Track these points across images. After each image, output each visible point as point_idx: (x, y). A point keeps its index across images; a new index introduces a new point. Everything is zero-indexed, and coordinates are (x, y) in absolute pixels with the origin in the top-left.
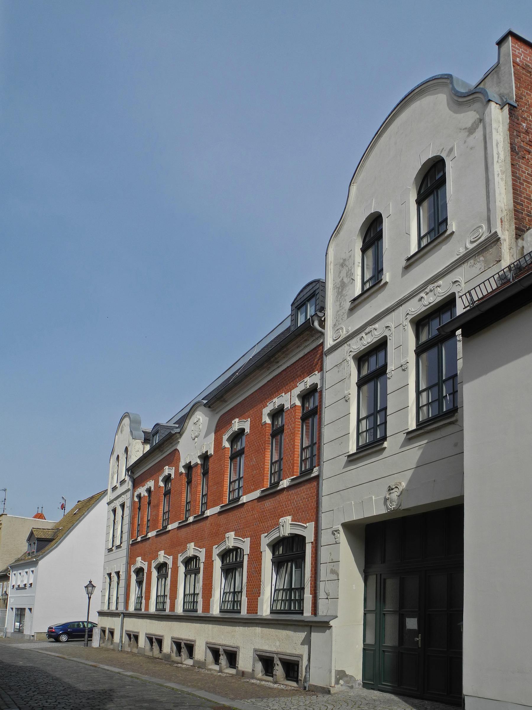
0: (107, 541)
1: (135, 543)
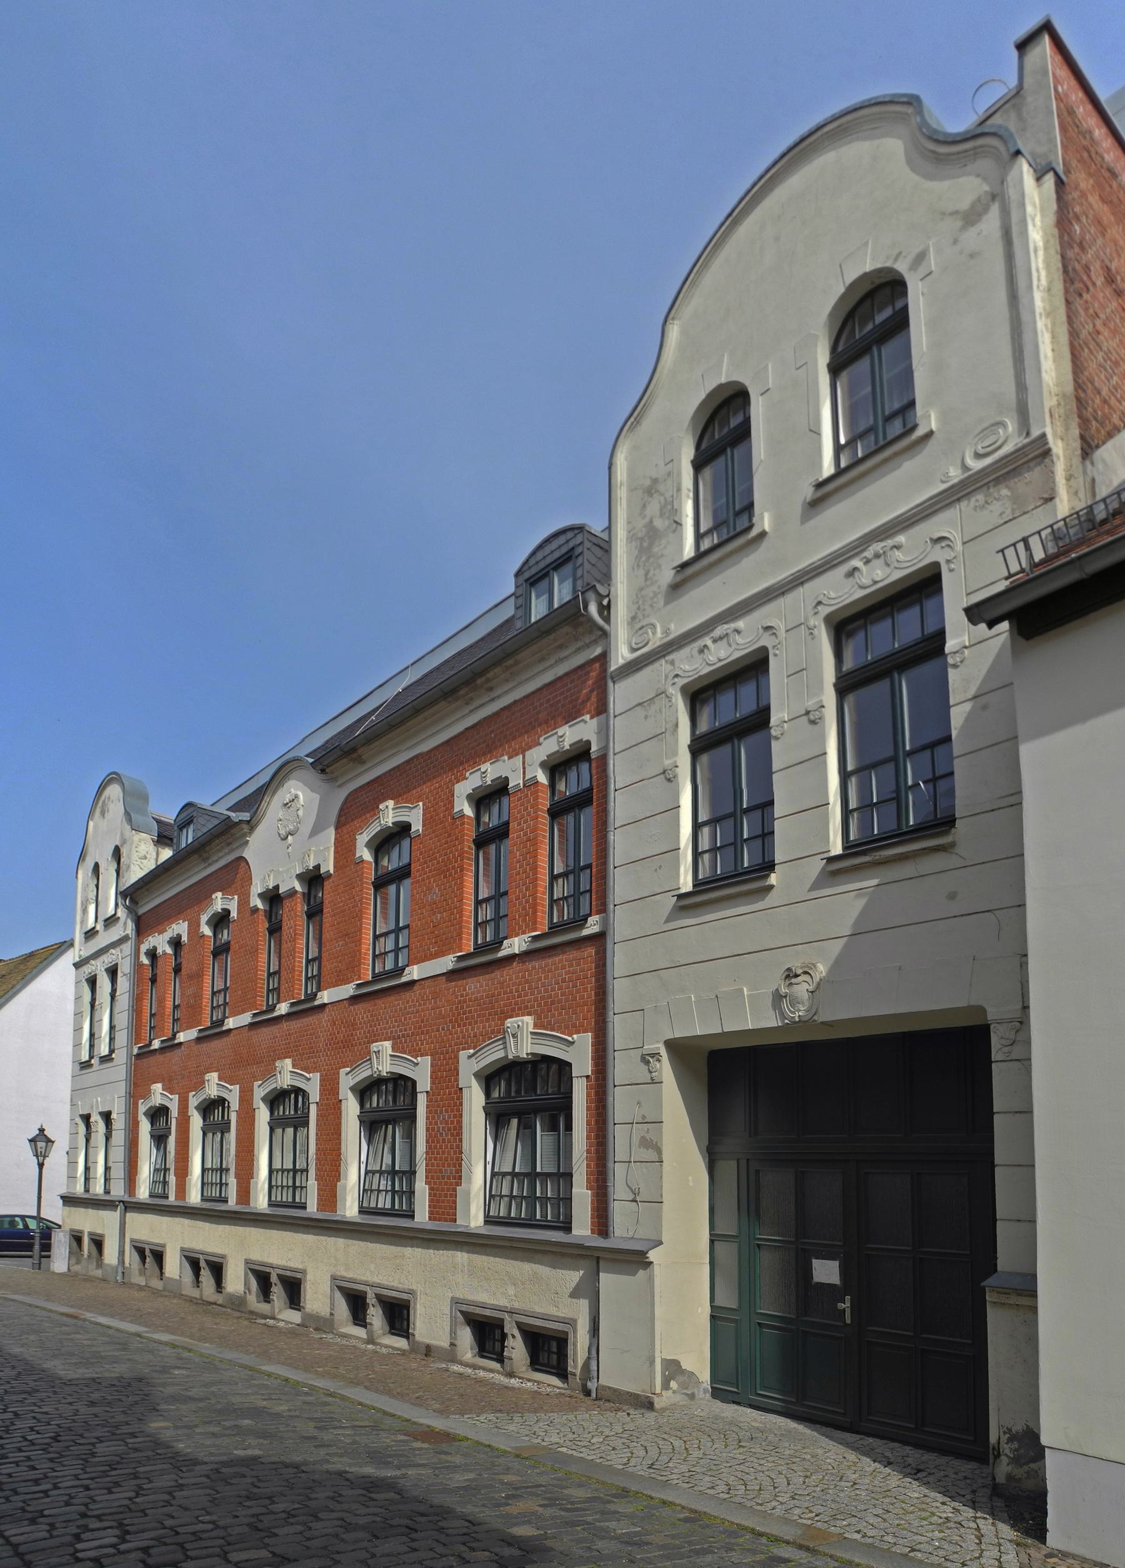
0: (77, 1045)
1: (145, 1053)
